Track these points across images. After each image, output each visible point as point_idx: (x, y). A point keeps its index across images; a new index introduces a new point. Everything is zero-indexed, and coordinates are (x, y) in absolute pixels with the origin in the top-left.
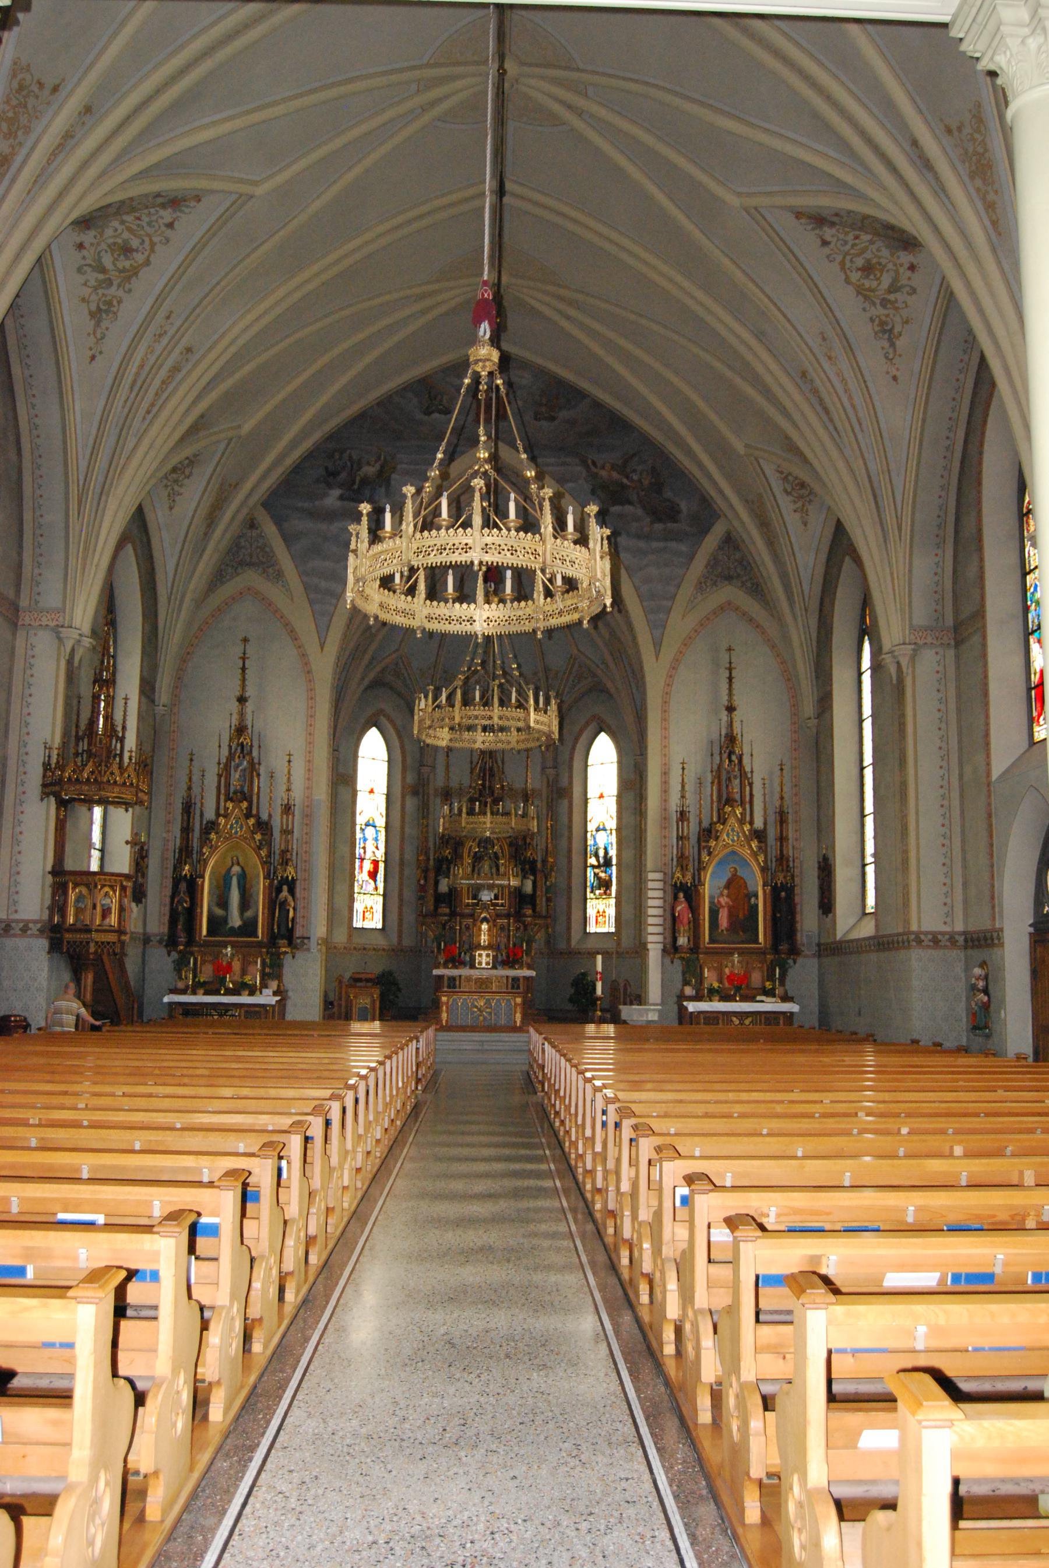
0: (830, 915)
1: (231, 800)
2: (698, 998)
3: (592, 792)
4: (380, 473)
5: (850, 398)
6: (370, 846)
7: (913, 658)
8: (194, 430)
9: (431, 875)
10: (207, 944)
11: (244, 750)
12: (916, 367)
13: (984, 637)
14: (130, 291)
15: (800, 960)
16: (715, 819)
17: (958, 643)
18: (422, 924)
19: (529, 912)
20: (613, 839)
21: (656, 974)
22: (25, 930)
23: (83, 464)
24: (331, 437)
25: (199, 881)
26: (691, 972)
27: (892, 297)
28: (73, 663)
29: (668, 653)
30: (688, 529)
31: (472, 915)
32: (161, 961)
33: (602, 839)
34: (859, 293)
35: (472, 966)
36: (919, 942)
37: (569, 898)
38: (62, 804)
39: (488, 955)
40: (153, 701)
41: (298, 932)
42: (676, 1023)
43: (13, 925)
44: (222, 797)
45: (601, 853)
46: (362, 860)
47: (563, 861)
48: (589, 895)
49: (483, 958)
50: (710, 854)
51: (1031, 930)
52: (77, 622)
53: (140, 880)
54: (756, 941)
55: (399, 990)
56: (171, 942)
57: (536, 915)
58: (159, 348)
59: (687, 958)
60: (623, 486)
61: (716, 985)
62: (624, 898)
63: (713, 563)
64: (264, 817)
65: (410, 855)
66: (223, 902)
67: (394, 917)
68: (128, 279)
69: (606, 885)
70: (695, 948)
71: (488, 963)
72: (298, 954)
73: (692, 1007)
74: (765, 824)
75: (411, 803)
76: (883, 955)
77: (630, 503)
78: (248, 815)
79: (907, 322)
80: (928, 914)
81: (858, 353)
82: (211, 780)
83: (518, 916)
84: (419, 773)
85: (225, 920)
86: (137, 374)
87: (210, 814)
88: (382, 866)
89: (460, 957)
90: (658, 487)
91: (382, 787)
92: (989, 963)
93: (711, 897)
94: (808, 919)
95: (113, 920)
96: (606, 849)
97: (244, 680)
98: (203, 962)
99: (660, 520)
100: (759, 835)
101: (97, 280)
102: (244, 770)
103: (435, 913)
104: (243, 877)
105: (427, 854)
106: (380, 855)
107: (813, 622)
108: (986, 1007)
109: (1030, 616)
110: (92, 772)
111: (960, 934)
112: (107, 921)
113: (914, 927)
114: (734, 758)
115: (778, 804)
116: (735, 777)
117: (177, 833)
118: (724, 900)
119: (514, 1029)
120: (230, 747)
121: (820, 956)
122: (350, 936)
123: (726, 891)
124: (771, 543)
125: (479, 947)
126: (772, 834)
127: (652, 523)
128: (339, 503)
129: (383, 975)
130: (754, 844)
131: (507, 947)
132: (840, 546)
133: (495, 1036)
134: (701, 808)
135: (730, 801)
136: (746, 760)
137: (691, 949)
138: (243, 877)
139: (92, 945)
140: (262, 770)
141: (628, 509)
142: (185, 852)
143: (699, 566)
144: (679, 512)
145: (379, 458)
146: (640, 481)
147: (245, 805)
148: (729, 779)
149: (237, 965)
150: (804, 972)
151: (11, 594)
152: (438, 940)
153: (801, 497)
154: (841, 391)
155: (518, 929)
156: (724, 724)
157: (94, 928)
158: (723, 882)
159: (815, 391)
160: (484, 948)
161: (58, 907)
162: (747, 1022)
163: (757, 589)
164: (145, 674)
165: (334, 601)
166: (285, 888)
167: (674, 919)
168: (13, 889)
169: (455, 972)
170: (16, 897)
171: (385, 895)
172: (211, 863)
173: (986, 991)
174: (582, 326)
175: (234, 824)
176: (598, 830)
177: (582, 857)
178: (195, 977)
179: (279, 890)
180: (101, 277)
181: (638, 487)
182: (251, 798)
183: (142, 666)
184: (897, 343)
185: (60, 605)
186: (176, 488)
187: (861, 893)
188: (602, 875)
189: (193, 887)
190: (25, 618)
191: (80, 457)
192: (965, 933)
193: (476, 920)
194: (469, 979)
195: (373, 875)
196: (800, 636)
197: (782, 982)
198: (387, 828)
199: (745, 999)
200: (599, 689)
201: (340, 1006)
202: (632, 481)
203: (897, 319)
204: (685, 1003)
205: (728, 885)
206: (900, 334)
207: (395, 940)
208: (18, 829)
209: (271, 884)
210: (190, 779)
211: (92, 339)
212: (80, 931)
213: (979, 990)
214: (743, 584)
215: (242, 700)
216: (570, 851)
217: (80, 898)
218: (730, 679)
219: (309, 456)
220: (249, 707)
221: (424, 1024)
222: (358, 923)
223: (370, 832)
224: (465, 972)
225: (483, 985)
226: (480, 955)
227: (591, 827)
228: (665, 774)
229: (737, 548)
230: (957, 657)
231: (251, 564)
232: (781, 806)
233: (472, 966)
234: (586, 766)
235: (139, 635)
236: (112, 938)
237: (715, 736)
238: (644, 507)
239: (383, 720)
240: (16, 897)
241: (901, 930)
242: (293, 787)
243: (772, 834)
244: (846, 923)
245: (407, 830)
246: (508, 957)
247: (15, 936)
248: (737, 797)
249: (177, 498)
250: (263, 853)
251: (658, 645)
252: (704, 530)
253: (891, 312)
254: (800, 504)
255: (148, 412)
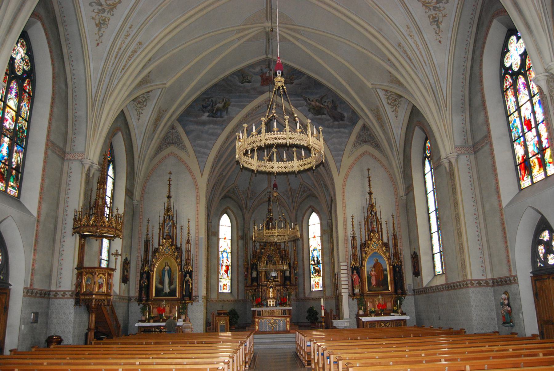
0: (419, 277)
1: (165, 239)
2: (365, 315)
3: (311, 235)
4: (224, 106)
5: (420, 52)
6: (225, 260)
7: (456, 160)
8: (144, 81)
9: (250, 271)
10: (155, 300)
11: (171, 218)
12: (450, 35)
13: (491, 145)
14: (113, 15)
15: (406, 297)
16: (367, 239)
17: (475, 152)
18: (246, 290)
19: (288, 283)
20: (320, 253)
21: (347, 306)
22: (64, 295)
23: (94, 90)
24: (205, 93)
25: (152, 273)
26: (361, 304)
27: (438, 5)
28: (89, 176)
29: (343, 173)
30: (348, 123)
31: (266, 286)
32: (135, 308)
33: (316, 254)
34: (423, 5)
35: (267, 306)
36: (472, 284)
37: (304, 277)
38: (83, 237)
39: (273, 301)
40: (132, 199)
41: (194, 294)
42: (356, 327)
43: (58, 293)
44: (161, 238)
45: (316, 259)
46: (222, 265)
47: (300, 263)
48: (312, 276)
49: (271, 303)
50: (366, 253)
51: (532, 275)
52: (91, 156)
53: (126, 273)
54: (388, 290)
55: (238, 317)
56: (140, 300)
57: (291, 284)
58: (127, 41)
59: (360, 298)
60: (321, 108)
61: (373, 309)
62: (326, 276)
63: (359, 136)
64: (179, 245)
65: (241, 263)
66: (162, 282)
67: (235, 287)
68: (112, 9)
69: (318, 271)
70: (362, 294)
71: (273, 305)
72: (194, 303)
73: (364, 319)
74: (388, 240)
75: (241, 242)
76: (451, 292)
77: (324, 114)
78: (172, 245)
79: (445, 16)
80: (474, 272)
81: (423, 32)
82: (156, 231)
83: (284, 285)
84: (243, 231)
85: (162, 290)
86: (118, 53)
87: (156, 245)
88: (230, 267)
89: (262, 303)
90: (335, 108)
91: (229, 237)
92: (509, 292)
93: (368, 272)
94: (409, 279)
95: (104, 289)
96: (317, 257)
97: (170, 189)
98: (153, 308)
99: (337, 120)
100: (386, 245)
101: (98, 9)
102: (170, 226)
103: (251, 285)
104: (170, 271)
105: (247, 262)
106: (229, 263)
107: (402, 158)
108: (510, 313)
109: (513, 134)
110: (94, 221)
111: (490, 280)
112: (101, 290)
113: (469, 278)
114: (373, 213)
115: (392, 231)
116: (374, 221)
117: (142, 253)
118: (373, 273)
119: (286, 332)
120: (164, 217)
121: (414, 295)
122: (218, 296)
123: (373, 269)
124: (382, 126)
125: (269, 298)
126: (391, 244)
127: (334, 121)
128: (208, 118)
129: (231, 311)
130: (384, 249)
131: (280, 297)
132: (416, 118)
133: (278, 336)
134: (361, 235)
135: (373, 231)
136: (378, 214)
137: (360, 294)
138: (170, 271)
139: (94, 301)
140: (178, 226)
141: (324, 116)
142: (146, 261)
143: (353, 137)
144: (344, 117)
145: (223, 101)
146: (328, 106)
147: (170, 240)
148: (372, 222)
149: (167, 309)
150: (408, 302)
151: (61, 145)
152: (253, 296)
153: (395, 105)
154: (416, 50)
155: (284, 290)
156: (368, 200)
157: (94, 293)
158: (372, 265)
159: (405, 52)
160: (271, 299)
161: (79, 284)
162: (387, 325)
163: (377, 146)
164: (128, 187)
165: (207, 157)
166: (188, 275)
167: (352, 281)
168: (59, 276)
169: (260, 309)
170: (60, 280)
171: (231, 279)
172: (157, 265)
173: (509, 305)
174: (303, 42)
175: (166, 249)
176: (314, 250)
177: (308, 261)
178: (149, 314)
179: (185, 276)
180: (100, 8)
181: (328, 107)
182: (173, 237)
183: (126, 183)
184: (441, 26)
185: (83, 150)
186: (140, 110)
187: (435, 264)
188: (317, 268)
189: (149, 277)
190: (68, 157)
191: (93, 86)
192: (492, 279)
193: (268, 288)
194: (266, 311)
195: (226, 271)
196: (396, 162)
197: (400, 308)
198: (231, 253)
199: (386, 315)
200: (312, 196)
201: (213, 324)
202: (324, 106)
203: (441, 15)
204: (360, 318)
205: (374, 267)
206: (442, 22)
207: (236, 297)
208: (62, 249)
209: (182, 274)
210: (148, 231)
211: (97, 36)
212: (87, 295)
213: (505, 305)
214: (371, 144)
215: (169, 197)
216: (303, 258)
217: (88, 279)
218: (369, 181)
219: (196, 101)
220: (172, 200)
221: (249, 333)
222: (221, 291)
223: (225, 254)
224: (264, 309)
225: (272, 314)
226: (270, 302)
227: (311, 249)
228: (345, 221)
229: (368, 130)
230: (476, 159)
231: (173, 143)
232: (394, 232)
233: (267, 306)
234: (308, 226)
235: (125, 171)
236: (104, 297)
237: (365, 205)
238: (330, 116)
239: (229, 211)
240: (60, 280)
241: (461, 279)
242: (190, 232)
243: (391, 244)
244: (426, 279)
245: (239, 253)
246: (281, 301)
247: (59, 298)
248: (376, 229)
249: (141, 115)
250: (178, 260)
251: (339, 169)
252: (354, 123)
253: (438, 12)
254: (394, 108)
255: (123, 69)
